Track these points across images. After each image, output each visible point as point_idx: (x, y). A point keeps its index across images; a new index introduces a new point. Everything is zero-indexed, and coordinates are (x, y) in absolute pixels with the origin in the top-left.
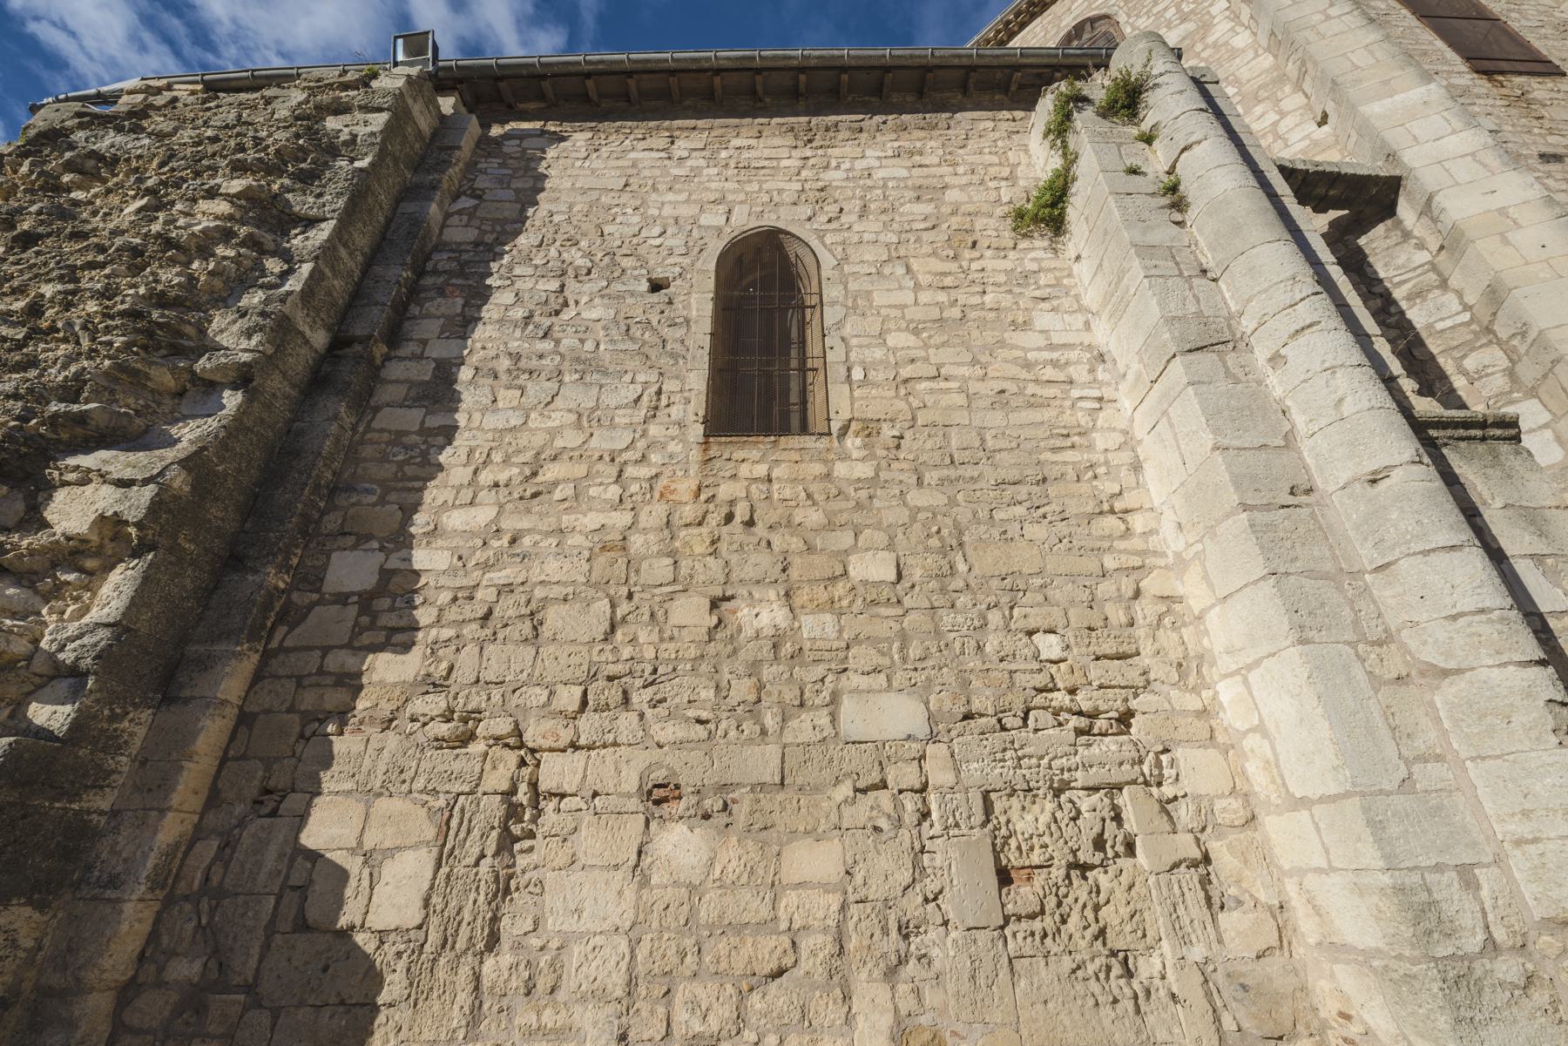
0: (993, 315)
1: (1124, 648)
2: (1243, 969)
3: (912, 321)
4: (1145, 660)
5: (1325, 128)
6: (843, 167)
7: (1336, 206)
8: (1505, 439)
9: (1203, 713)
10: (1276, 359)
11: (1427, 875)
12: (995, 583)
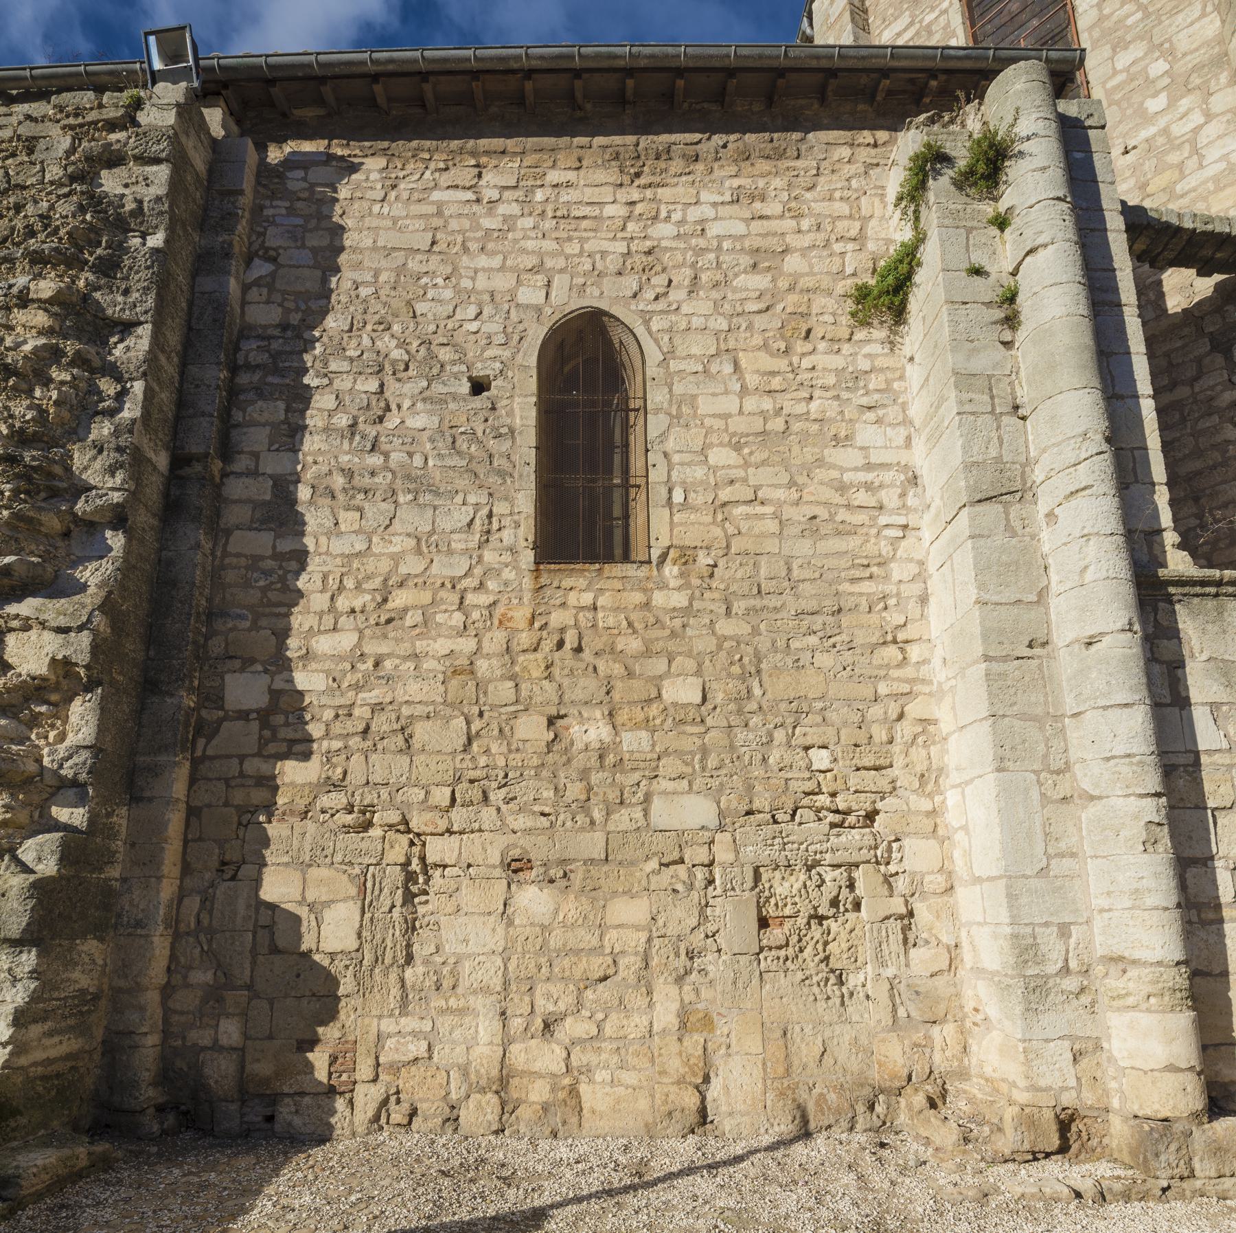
0: (816, 427)
3: (734, 434)
4: (895, 772)
9: (933, 813)
10: (1051, 515)
12: (783, 706)
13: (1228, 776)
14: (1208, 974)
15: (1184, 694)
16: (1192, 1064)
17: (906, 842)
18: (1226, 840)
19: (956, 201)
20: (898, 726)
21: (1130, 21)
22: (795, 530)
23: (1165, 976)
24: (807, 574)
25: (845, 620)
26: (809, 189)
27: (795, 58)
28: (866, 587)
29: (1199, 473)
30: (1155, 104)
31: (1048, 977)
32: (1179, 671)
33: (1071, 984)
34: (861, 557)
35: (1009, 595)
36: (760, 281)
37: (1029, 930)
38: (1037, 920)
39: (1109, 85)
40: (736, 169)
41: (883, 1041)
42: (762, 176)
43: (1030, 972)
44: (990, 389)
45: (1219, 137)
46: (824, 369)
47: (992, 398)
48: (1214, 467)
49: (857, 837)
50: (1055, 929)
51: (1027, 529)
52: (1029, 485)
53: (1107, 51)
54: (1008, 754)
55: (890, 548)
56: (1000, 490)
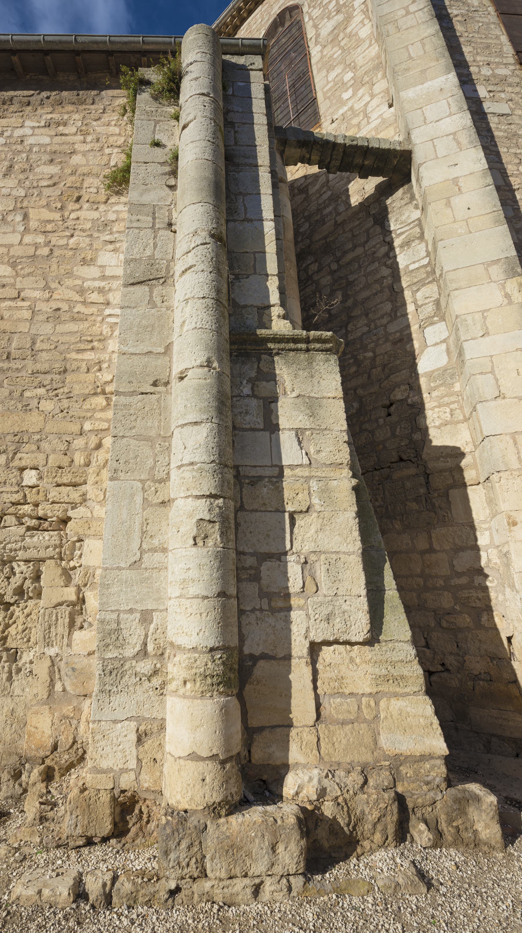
0: (71, 253)
1: (78, 480)
2: (76, 660)
3: (13, 256)
4: (88, 488)
5: (392, 109)
6: (6, 134)
7: (376, 174)
8: (322, 351)
12: (10, 438)
13: (306, 486)
14: (273, 658)
15: (274, 422)
16: (215, 752)
17: (87, 542)
18: (300, 538)
19: (152, 106)
20: (96, 453)
21: (335, 56)
22: (41, 318)
23: (198, 662)
24: (45, 346)
25: (69, 378)
26: (96, 120)
27: (82, 43)
28: (89, 356)
29: (368, 298)
30: (346, 96)
31: (124, 660)
32: (273, 405)
33: (145, 667)
34: (87, 335)
35: (143, 348)
36: (53, 169)
37: (114, 616)
38: (124, 607)
39: (325, 90)
40: (52, 109)
41: (36, 713)
42: (68, 113)
43: (109, 655)
44: (154, 213)
45: (378, 106)
46: (85, 219)
47: (154, 218)
48: (376, 294)
49: (47, 538)
50: (138, 615)
51: (166, 303)
52: (171, 274)
53: (324, 73)
54: (122, 466)
55: (109, 329)
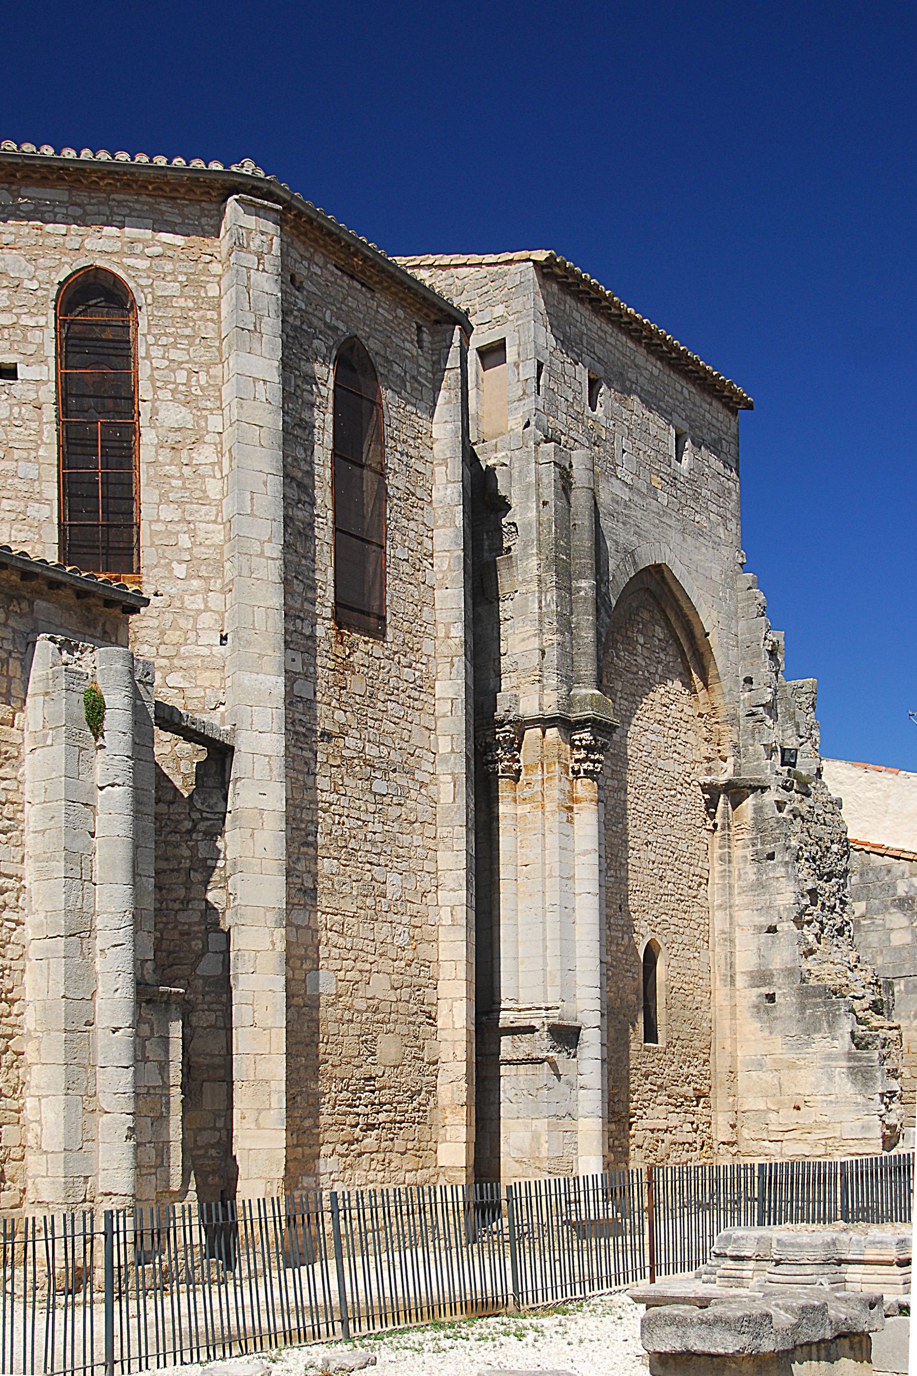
9: (18, 1111)
11: (305, 604)
56: (79, 932)
